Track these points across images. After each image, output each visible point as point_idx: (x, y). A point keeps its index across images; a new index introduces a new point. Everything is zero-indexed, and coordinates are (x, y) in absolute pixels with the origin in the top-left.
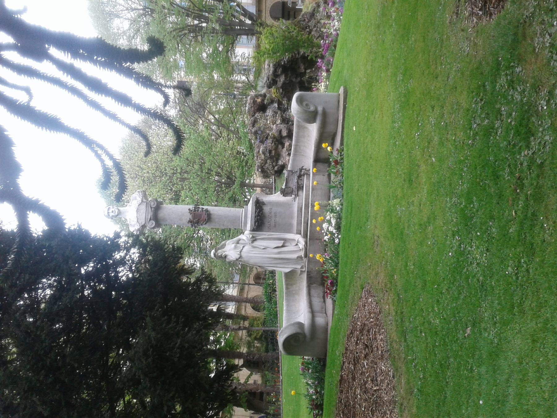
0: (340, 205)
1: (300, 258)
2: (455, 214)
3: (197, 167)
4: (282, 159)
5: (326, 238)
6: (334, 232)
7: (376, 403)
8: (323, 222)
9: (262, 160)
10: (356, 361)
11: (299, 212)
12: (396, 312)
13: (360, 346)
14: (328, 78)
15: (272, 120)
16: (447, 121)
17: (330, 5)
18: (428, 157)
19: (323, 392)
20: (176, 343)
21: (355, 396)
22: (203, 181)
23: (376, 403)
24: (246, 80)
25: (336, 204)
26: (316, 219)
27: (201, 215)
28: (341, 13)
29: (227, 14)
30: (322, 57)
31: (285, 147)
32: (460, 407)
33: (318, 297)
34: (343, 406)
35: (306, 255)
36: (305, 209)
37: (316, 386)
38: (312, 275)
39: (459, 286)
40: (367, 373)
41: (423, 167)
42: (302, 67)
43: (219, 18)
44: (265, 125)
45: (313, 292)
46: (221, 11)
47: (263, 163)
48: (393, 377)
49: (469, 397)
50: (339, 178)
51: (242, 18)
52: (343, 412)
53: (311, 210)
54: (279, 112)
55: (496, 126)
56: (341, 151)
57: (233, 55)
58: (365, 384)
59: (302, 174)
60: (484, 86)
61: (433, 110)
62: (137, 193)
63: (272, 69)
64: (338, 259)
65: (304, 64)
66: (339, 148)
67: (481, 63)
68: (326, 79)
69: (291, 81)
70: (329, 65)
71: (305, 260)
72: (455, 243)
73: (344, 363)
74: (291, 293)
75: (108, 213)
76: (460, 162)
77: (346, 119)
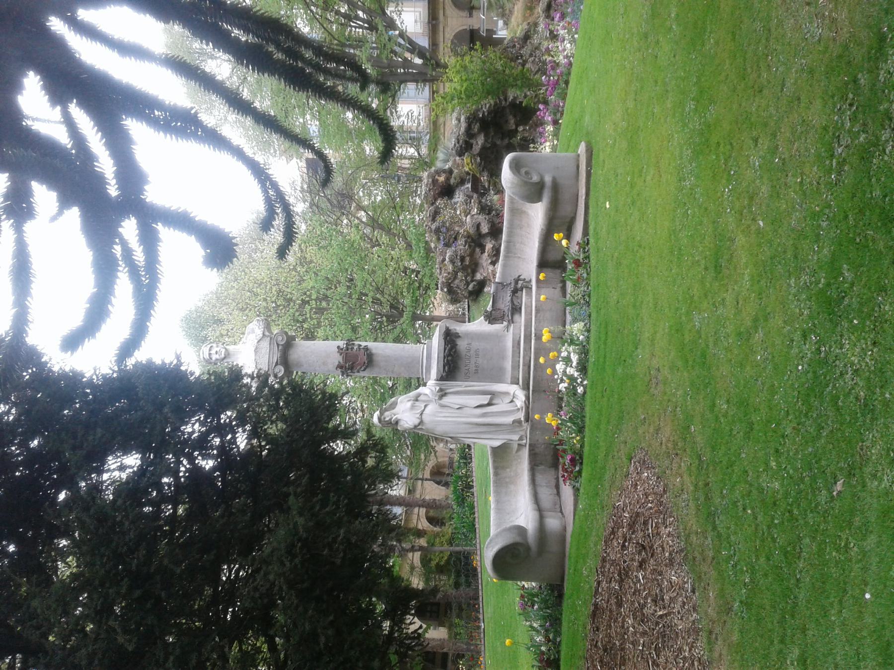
0: (585, 331)
1: (518, 422)
2: (807, 302)
3: (342, 289)
4: (481, 271)
5: (562, 386)
6: (576, 376)
7: (664, 636)
8: (556, 360)
9: (449, 273)
10: (624, 575)
11: (515, 349)
12: (696, 486)
13: (631, 549)
14: (556, 134)
15: (464, 209)
16: (787, 156)
17: (557, 19)
18: (750, 222)
19: (558, 640)
20: (339, 536)
21: (623, 631)
22: (351, 311)
23: (664, 636)
24: (416, 154)
25: (579, 330)
26: (546, 356)
27: (356, 356)
28: (576, 29)
29: (384, 49)
30: (546, 103)
31: (486, 251)
32: (825, 613)
33: (547, 486)
34: (601, 652)
35: (527, 419)
36: (524, 342)
37: (547, 631)
38: (537, 450)
39: (819, 416)
40: (644, 590)
41: (741, 240)
42: (512, 121)
43: (372, 57)
44: (452, 217)
45: (539, 478)
46: (374, 45)
47: (450, 279)
48: (693, 591)
49: (843, 592)
50: (582, 289)
51: (408, 55)
52: (601, 661)
53: (535, 344)
54: (475, 196)
55: (883, 139)
56: (584, 245)
57: (394, 114)
58: (642, 609)
59: (518, 287)
60: (855, 81)
61: (756, 145)
62: (255, 322)
63: (463, 125)
64: (582, 421)
65: (515, 116)
66: (581, 242)
67: (846, 47)
68: (553, 136)
69: (494, 145)
70: (558, 112)
71: (526, 426)
72: (808, 349)
73: (599, 583)
74: (502, 482)
75: (210, 354)
76: (815, 216)
77: (592, 193)
